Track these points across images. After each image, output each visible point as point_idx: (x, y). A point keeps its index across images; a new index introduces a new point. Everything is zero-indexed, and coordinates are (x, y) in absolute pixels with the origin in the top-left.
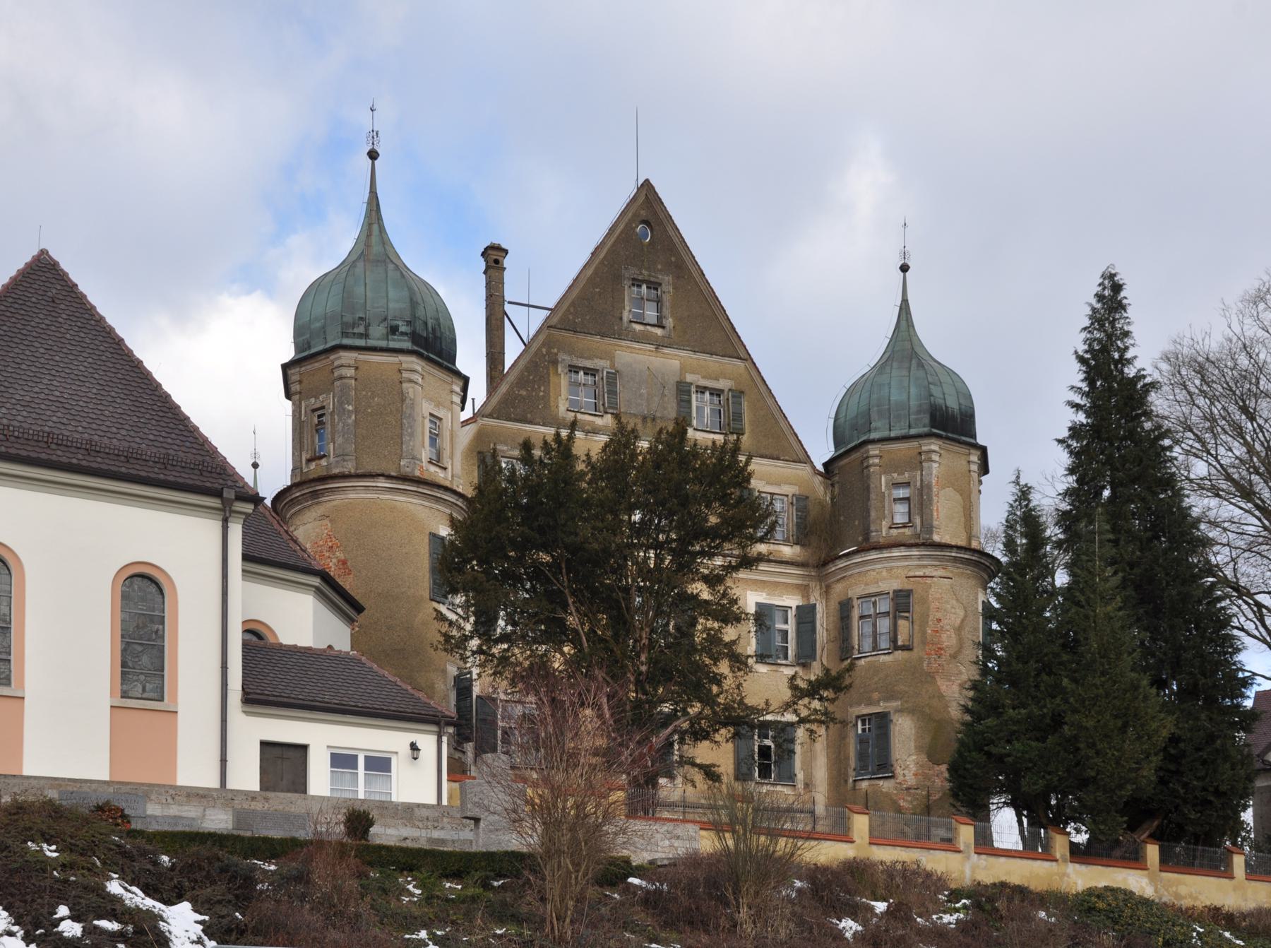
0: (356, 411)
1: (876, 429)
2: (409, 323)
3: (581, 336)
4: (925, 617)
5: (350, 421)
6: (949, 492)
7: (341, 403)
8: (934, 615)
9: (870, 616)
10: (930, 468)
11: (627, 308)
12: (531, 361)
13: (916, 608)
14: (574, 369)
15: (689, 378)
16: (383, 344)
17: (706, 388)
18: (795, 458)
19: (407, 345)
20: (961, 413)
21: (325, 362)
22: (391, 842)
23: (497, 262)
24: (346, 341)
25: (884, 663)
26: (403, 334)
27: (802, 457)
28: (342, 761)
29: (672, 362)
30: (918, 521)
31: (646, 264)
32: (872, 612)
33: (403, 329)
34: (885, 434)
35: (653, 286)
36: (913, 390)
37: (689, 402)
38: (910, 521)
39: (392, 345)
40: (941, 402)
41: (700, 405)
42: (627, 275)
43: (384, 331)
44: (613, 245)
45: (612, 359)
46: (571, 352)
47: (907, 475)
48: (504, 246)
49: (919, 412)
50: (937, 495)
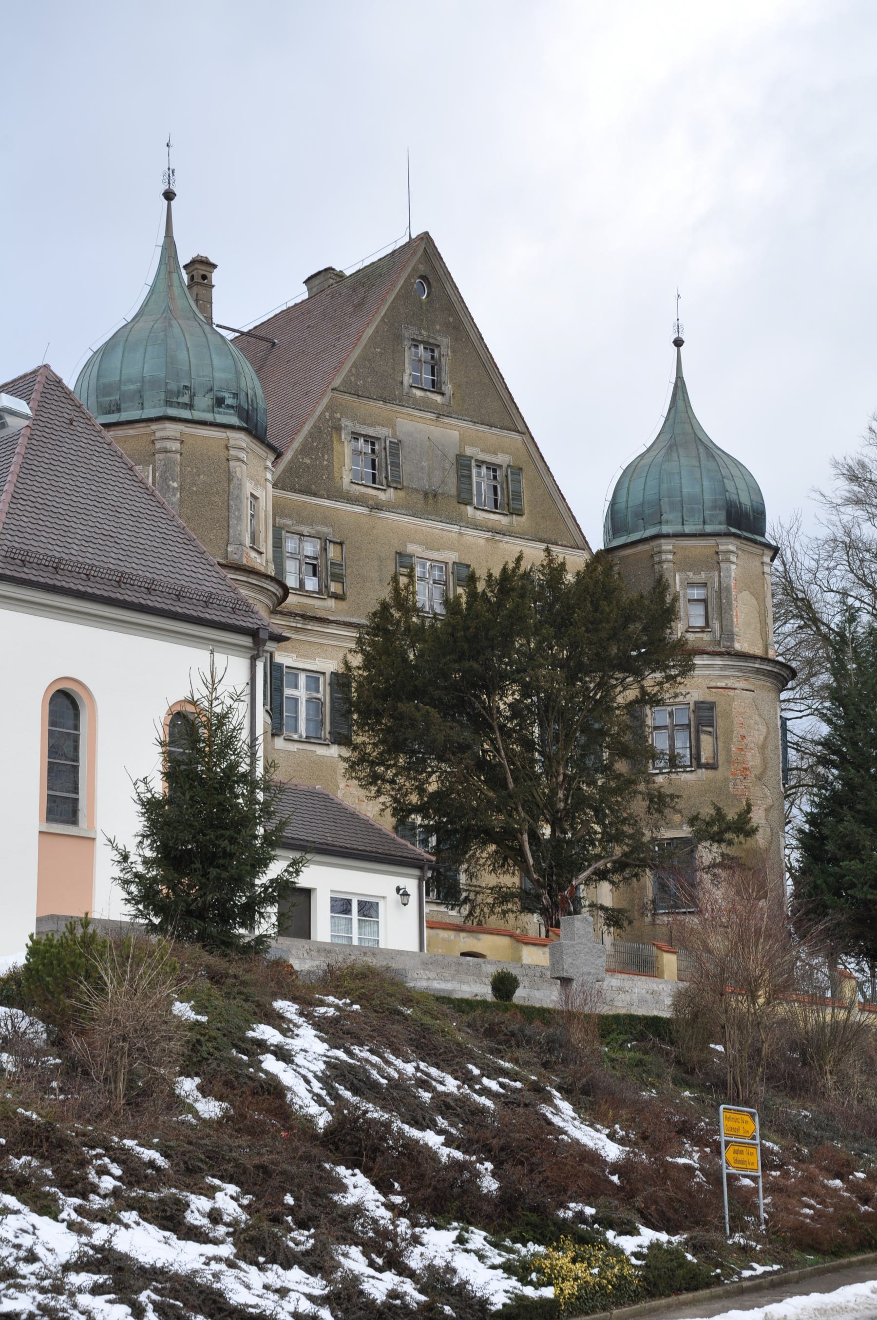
0: (181, 488)
1: (667, 522)
2: (236, 395)
3: (363, 401)
4: (729, 732)
5: (174, 499)
6: (746, 594)
7: (165, 480)
8: (738, 731)
9: (665, 727)
10: (728, 570)
11: (408, 371)
12: (315, 426)
13: (720, 723)
14: (356, 436)
15: (469, 451)
16: (208, 417)
17: (483, 462)
18: (572, 543)
19: (234, 420)
20: (753, 511)
21: (148, 430)
22: (467, 996)
23: (204, 277)
24: (172, 412)
25: (686, 782)
26: (229, 407)
27: (580, 543)
28: (341, 906)
29: (452, 433)
30: (716, 625)
31: (425, 323)
32: (668, 722)
33: (229, 401)
34: (678, 528)
35: (431, 347)
36: (706, 483)
37: (470, 477)
38: (707, 624)
39: (220, 419)
40: (734, 497)
41: (479, 480)
42: (407, 335)
43: (210, 403)
44: (393, 302)
45: (393, 426)
46: (354, 418)
47: (703, 574)
48: (212, 260)
49: (714, 508)
50: (736, 600)
